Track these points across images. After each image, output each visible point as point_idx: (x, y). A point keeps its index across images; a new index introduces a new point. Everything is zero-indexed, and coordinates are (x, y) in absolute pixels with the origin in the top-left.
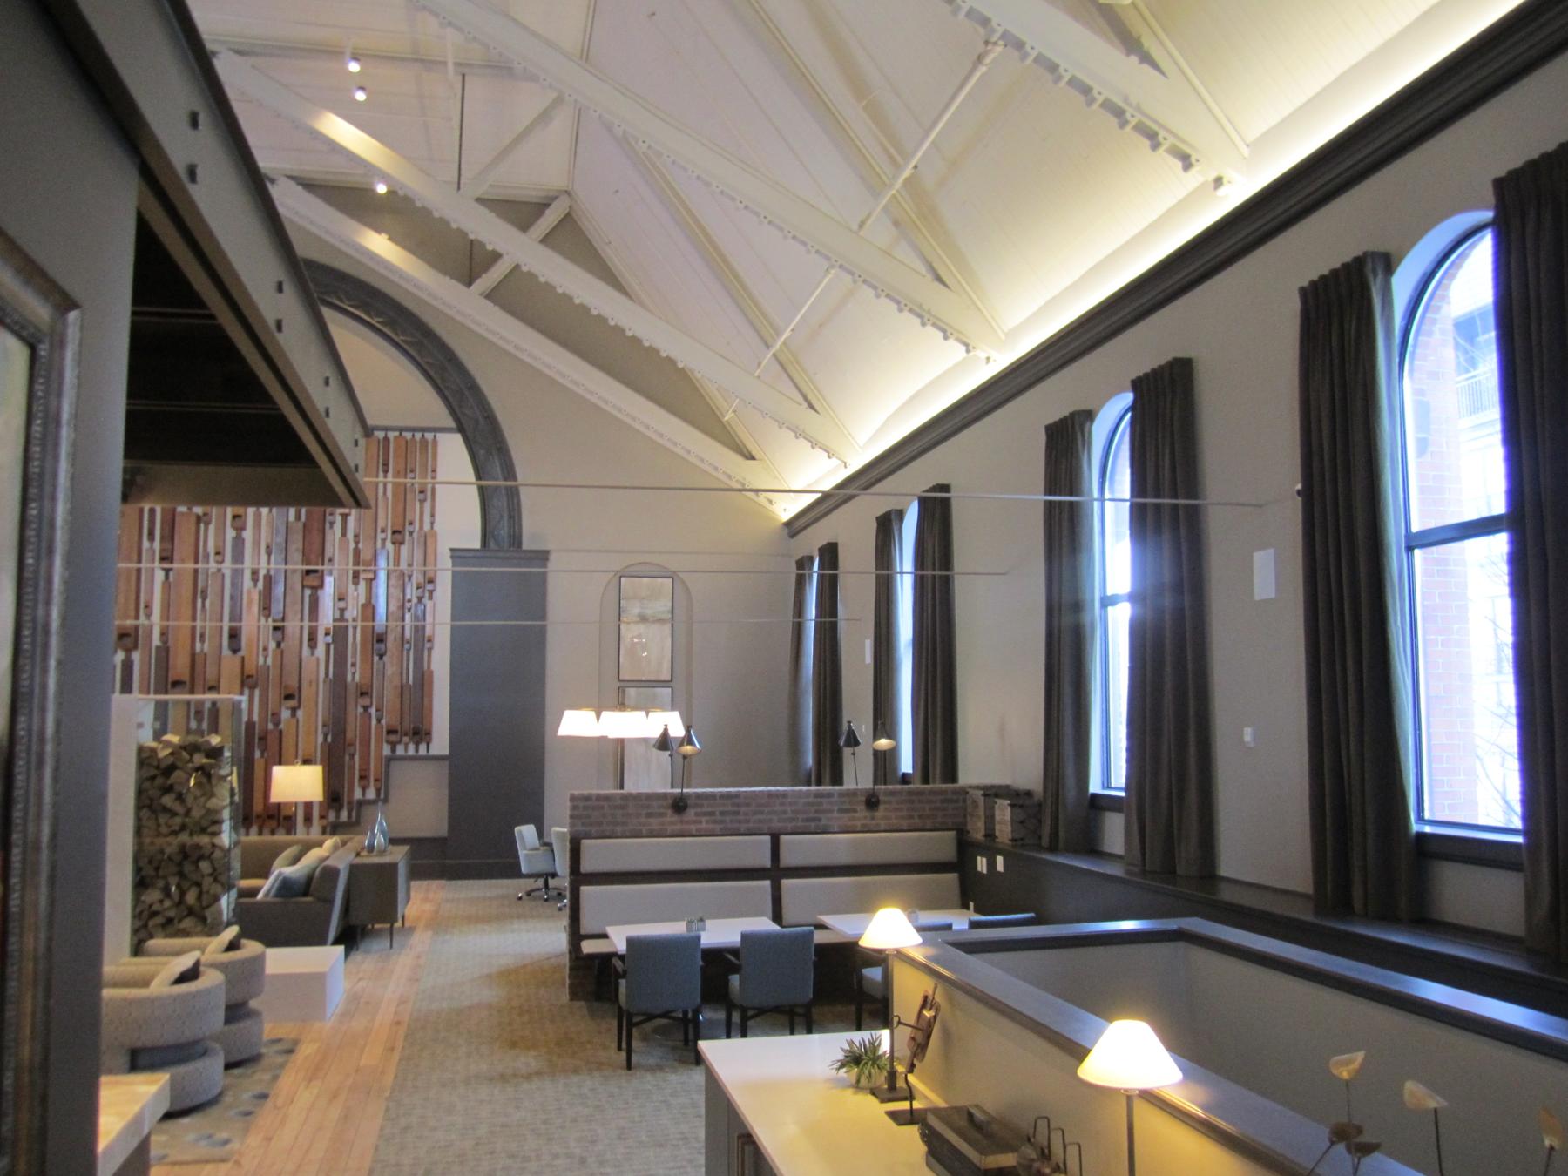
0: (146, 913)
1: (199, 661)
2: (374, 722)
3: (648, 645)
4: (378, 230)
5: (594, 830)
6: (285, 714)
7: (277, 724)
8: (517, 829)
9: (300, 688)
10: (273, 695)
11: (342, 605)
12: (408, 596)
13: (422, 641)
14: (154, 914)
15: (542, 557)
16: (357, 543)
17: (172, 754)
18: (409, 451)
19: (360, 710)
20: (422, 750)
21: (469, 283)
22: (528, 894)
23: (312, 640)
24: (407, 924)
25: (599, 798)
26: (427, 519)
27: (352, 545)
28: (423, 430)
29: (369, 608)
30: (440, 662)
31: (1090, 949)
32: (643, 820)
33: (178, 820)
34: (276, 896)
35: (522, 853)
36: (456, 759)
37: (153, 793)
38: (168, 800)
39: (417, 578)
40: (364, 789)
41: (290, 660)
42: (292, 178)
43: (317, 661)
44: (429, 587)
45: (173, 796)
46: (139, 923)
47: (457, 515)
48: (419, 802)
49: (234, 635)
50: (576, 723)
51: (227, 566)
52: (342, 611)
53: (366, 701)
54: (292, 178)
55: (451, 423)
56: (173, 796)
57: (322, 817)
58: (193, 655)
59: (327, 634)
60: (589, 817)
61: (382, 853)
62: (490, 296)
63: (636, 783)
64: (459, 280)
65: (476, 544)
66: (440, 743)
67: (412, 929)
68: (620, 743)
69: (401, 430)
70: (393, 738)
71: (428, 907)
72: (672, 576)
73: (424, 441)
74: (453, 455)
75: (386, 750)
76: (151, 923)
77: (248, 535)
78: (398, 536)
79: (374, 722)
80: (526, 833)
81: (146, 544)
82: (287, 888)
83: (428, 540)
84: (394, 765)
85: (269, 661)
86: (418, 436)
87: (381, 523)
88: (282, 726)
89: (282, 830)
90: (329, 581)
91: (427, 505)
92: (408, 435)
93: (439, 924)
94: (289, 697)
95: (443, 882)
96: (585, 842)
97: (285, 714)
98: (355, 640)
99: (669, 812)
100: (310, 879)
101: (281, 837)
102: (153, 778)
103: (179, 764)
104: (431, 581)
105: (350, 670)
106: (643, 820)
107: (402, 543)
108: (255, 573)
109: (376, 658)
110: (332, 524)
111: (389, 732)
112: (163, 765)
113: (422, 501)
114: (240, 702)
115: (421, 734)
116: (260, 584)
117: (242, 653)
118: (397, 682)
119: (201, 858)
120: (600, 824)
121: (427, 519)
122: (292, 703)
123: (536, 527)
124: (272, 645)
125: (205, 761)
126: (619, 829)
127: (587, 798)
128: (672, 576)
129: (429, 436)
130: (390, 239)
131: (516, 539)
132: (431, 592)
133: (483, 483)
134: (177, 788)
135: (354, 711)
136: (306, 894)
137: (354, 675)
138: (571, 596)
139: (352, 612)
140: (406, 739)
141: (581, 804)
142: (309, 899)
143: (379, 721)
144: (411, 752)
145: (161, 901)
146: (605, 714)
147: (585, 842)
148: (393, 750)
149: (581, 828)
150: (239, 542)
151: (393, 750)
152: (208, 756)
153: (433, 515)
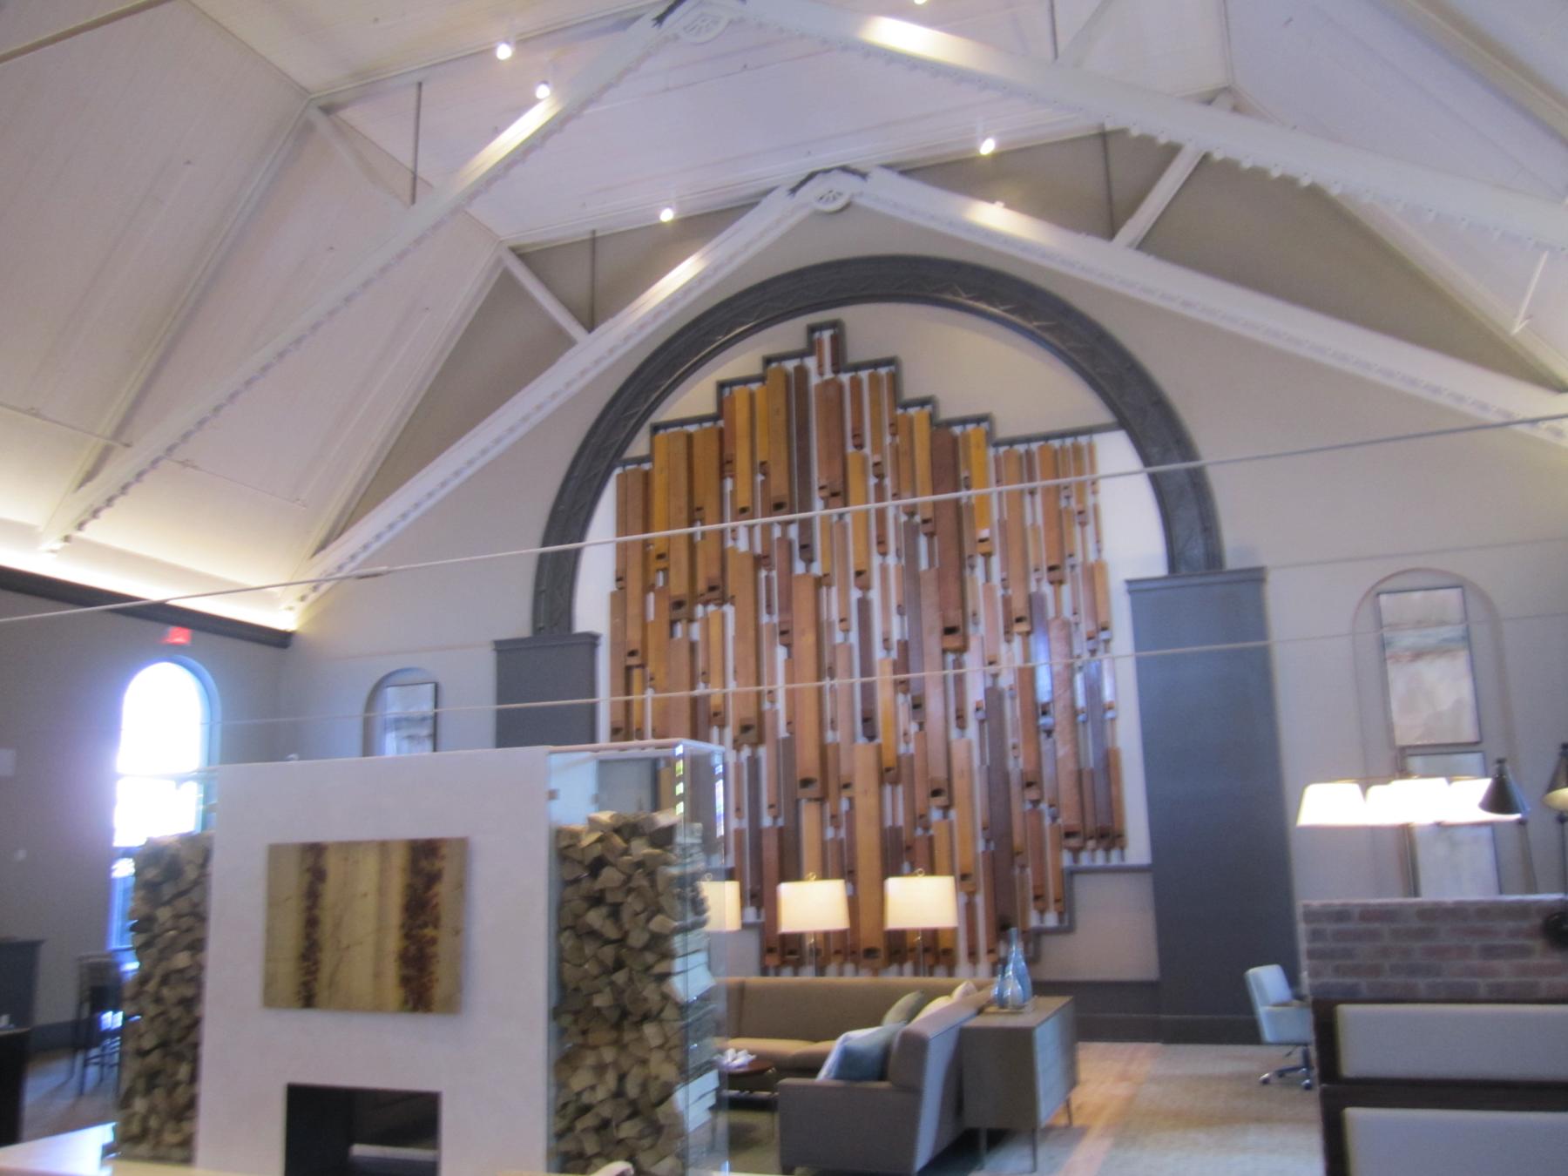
0: (571, 1109)
1: (830, 753)
2: (1047, 821)
3: (1440, 691)
4: (991, 199)
5: (1364, 984)
6: (936, 815)
7: (926, 828)
8: (1252, 971)
9: (949, 780)
10: (921, 792)
11: (992, 669)
12: (1077, 651)
13: (1098, 713)
14: (585, 1109)
15: (1255, 577)
16: (1005, 588)
17: (599, 840)
18: (1057, 458)
19: (1028, 806)
20: (1115, 858)
21: (1110, 232)
22: (1281, 1074)
23: (961, 718)
24: (1077, 1122)
25: (1369, 914)
26: (1091, 546)
27: (999, 593)
28: (1075, 433)
29: (1027, 676)
30: (1127, 736)
31: (11, 594)
32: (1475, 962)
33: (608, 953)
34: (837, 1077)
35: (1262, 1011)
36: (1165, 874)
37: (578, 905)
38: (595, 918)
39: (1085, 627)
40: (1042, 912)
41: (936, 745)
42: (888, 167)
43: (969, 742)
44: (1103, 635)
45: (604, 910)
46: (562, 1124)
47: (1128, 530)
48: (1114, 933)
49: (868, 720)
50: (1326, 805)
51: (854, 637)
52: (995, 676)
53: (1032, 794)
54: (888, 167)
55: (1105, 416)
56: (604, 910)
57: (990, 951)
58: (823, 749)
59: (977, 709)
60: (1348, 954)
61: (1018, 1009)
62: (1144, 245)
63: (1439, 888)
64: (1091, 230)
65: (1159, 569)
66: (1138, 848)
67: (1082, 1132)
68: (1405, 834)
69: (875, 364)
70: (1073, 842)
71: (1122, 1090)
72: (1459, 585)
73: (1077, 450)
74: (1115, 453)
75: (1066, 859)
76: (580, 1125)
77: (875, 595)
78: (1055, 574)
79: (1047, 821)
80: (1267, 980)
81: (765, 618)
82: (851, 1063)
83: (1094, 574)
84: (1078, 879)
85: (912, 746)
86: (1069, 441)
87: (1032, 564)
88: (932, 832)
89: (788, 970)
90: (974, 644)
91: (1090, 529)
92: (1056, 443)
93: (1131, 1125)
94: (936, 793)
95: (1157, 1046)
96: (1346, 1011)
97: (936, 815)
98: (1012, 711)
99: (1538, 944)
100: (886, 1050)
101: (939, 979)
102: (576, 881)
103: (610, 858)
104: (1104, 629)
105: (1011, 754)
106: (1475, 962)
107: (1061, 582)
108: (886, 641)
109: (1043, 736)
110: (972, 567)
111: (1069, 835)
112: (589, 858)
113: (1083, 524)
114: (709, 756)
115: (1111, 837)
116: (894, 654)
117: (878, 741)
118: (1070, 766)
119: (646, 1017)
120: (1375, 970)
121: (1091, 546)
122: (941, 800)
123: (1242, 536)
124: (914, 728)
125: (648, 850)
126: (1421, 983)
127: (1342, 915)
128: (1459, 585)
129: (1083, 440)
130: (1009, 206)
131: (1214, 559)
132: (1107, 642)
133: (1261, 643)
134: (610, 898)
135: (1020, 806)
136: (882, 1077)
137: (1016, 765)
138: (1306, 626)
139: (1006, 680)
140: (1091, 844)
141: (1330, 927)
142: (884, 1085)
143: (1054, 819)
144: (1100, 860)
145: (593, 1088)
146: (1375, 790)
147: (1346, 1011)
148: (1076, 859)
149: (1329, 979)
150: (864, 605)
151: (1076, 859)
152: (654, 844)
153: (1098, 541)
